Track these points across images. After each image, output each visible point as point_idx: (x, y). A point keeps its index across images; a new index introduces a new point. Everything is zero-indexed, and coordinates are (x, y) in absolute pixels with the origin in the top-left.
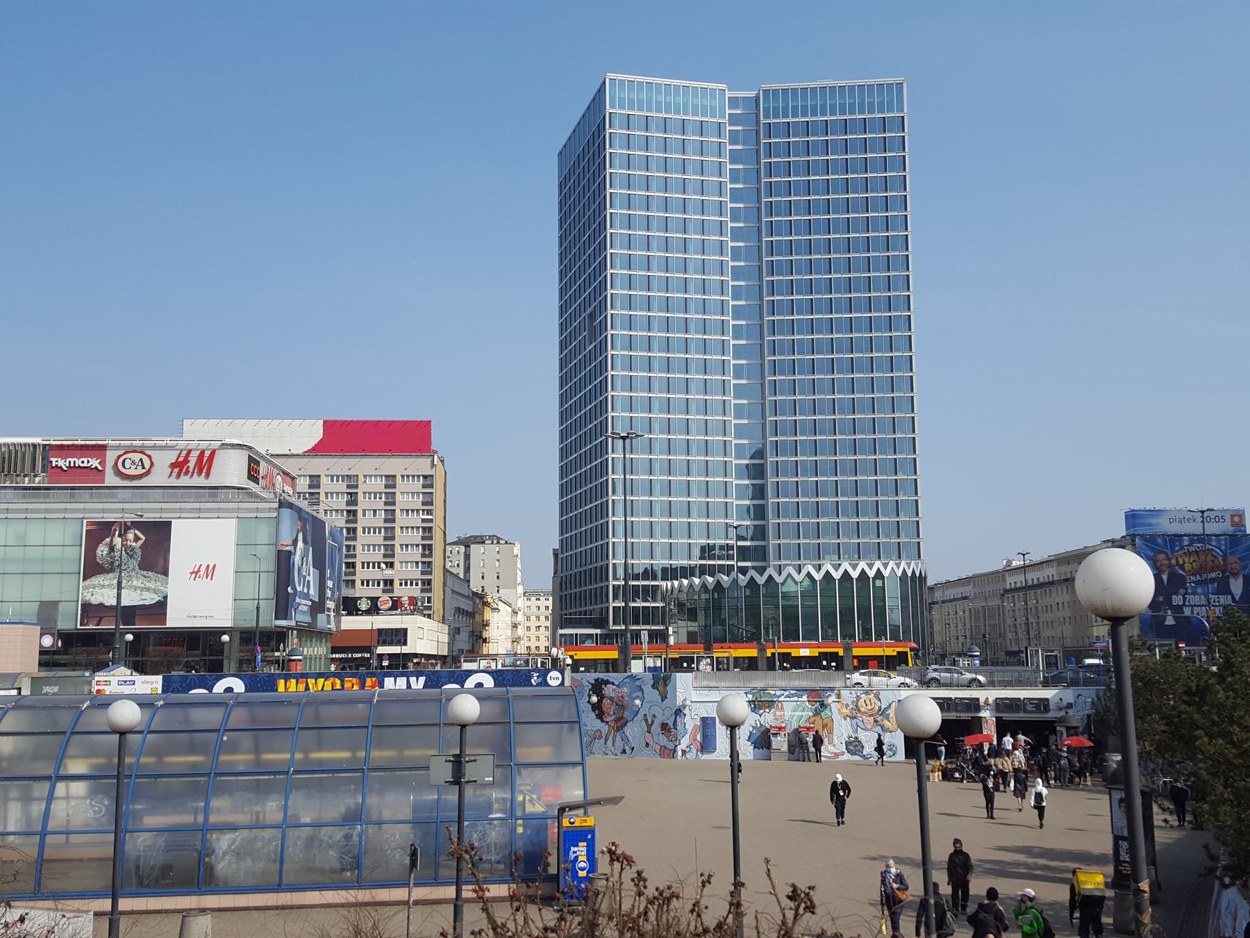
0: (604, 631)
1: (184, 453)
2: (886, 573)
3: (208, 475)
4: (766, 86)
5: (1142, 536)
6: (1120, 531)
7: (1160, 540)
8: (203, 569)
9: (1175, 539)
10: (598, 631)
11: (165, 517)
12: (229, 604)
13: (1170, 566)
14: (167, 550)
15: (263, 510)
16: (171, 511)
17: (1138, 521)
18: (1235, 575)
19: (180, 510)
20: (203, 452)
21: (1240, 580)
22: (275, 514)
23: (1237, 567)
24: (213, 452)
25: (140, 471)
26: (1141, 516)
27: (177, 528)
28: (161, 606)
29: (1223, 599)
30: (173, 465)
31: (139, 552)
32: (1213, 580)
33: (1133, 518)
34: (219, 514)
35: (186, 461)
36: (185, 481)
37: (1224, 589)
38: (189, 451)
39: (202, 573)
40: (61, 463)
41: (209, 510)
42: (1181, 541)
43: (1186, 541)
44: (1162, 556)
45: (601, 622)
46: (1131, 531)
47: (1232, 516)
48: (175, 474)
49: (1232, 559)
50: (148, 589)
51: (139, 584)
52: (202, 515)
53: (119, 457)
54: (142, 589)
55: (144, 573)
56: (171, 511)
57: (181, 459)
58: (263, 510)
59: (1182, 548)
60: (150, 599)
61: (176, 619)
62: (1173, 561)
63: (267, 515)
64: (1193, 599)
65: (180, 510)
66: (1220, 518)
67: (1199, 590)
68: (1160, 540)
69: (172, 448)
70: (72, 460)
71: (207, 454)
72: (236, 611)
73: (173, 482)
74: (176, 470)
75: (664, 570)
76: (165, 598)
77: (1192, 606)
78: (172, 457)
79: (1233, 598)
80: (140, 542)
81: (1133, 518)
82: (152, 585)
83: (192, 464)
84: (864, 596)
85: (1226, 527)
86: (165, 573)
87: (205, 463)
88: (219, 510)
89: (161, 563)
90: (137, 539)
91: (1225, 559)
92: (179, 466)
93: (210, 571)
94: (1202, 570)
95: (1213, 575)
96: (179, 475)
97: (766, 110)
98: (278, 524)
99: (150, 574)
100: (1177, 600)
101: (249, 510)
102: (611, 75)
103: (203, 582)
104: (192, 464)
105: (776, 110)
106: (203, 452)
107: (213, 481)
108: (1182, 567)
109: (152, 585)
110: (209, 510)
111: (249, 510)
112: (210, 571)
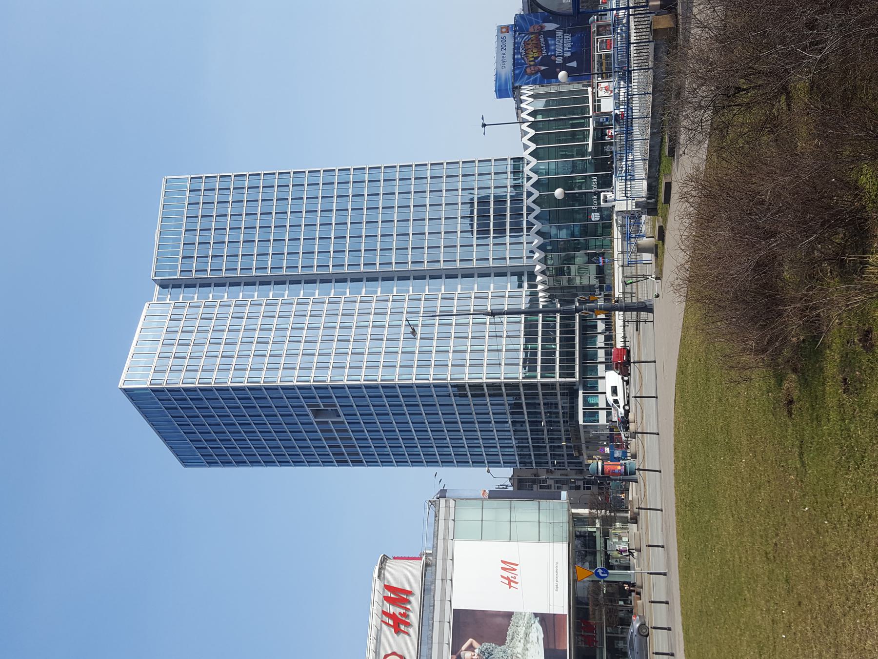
0: (581, 387)
1: (386, 619)
2: (531, 109)
3: (410, 593)
4: (152, 276)
5: (513, 83)
6: (510, 102)
7: (517, 72)
8: (506, 574)
9: (516, 63)
10: (581, 392)
11: (449, 617)
12: (544, 547)
13: (535, 65)
14: (484, 612)
15: (447, 513)
16: (442, 611)
17: (503, 88)
18: (542, 28)
19: (443, 601)
20: (386, 599)
21: (546, 24)
22: (452, 502)
23: (536, 27)
24: (387, 587)
26: (500, 86)
27: (460, 603)
28: (547, 621)
29: (559, 33)
30: (397, 631)
31: (486, 645)
32: (546, 41)
33: (501, 92)
34: (448, 559)
35: (393, 616)
36: (414, 618)
37: (552, 34)
38: (384, 613)
39: (510, 575)
41: (444, 570)
42: (518, 59)
43: (518, 56)
44: (528, 70)
45: (571, 391)
46: (510, 93)
47: (502, 32)
48: (407, 629)
49: (531, 30)
50: (527, 635)
51: (521, 645)
52: (449, 578)
54: (527, 641)
55: (508, 639)
56: (442, 611)
57: (391, 622)
58: (447, 513)
59: (523, 58)
60: (537, 632)
61: (559, 604)
62: (532, 63)
63: (452, 510)
64: (559, 51)
65: (443, 601)
66: (503, 40)
67: (553, 48)
68: (517, 72)
69: (379, 632)
71: (388, 594)
72: (552, 539)
73: (414, 631)
74: (402, 627)
75: (527, 341)
76: (536, 615)
77: (564, 51)
78: (388, 632)
79: (557, 29)
80: (475, 644)
81: (501, 92)
82: (522, 630)
83: (397, 610)
84: (547, 124)
85: (509, 37)
86: (509, 615)
87: (398, 596)
88: (445, 559)
89: (499, 620)
90: (471, 648)
91: (532, 34)
92: (398, 624)
93: (509, 566)
94: (538, 46)
95: (542, 40)
96: (408, 624)
97: (170, 274)
98: (462, 499)
99: (510, 632)
100: (559, 60)
101: (446, 528)
102: (121, 382)
103: (521, 574)
104: (397, 610)
105: (171, 267)
106: (386, 599)
107: (416, 588)
108: (536, 58)
109: (522, 630)
110: (444, 570)
111: (446, 528)
112: (509, 566)
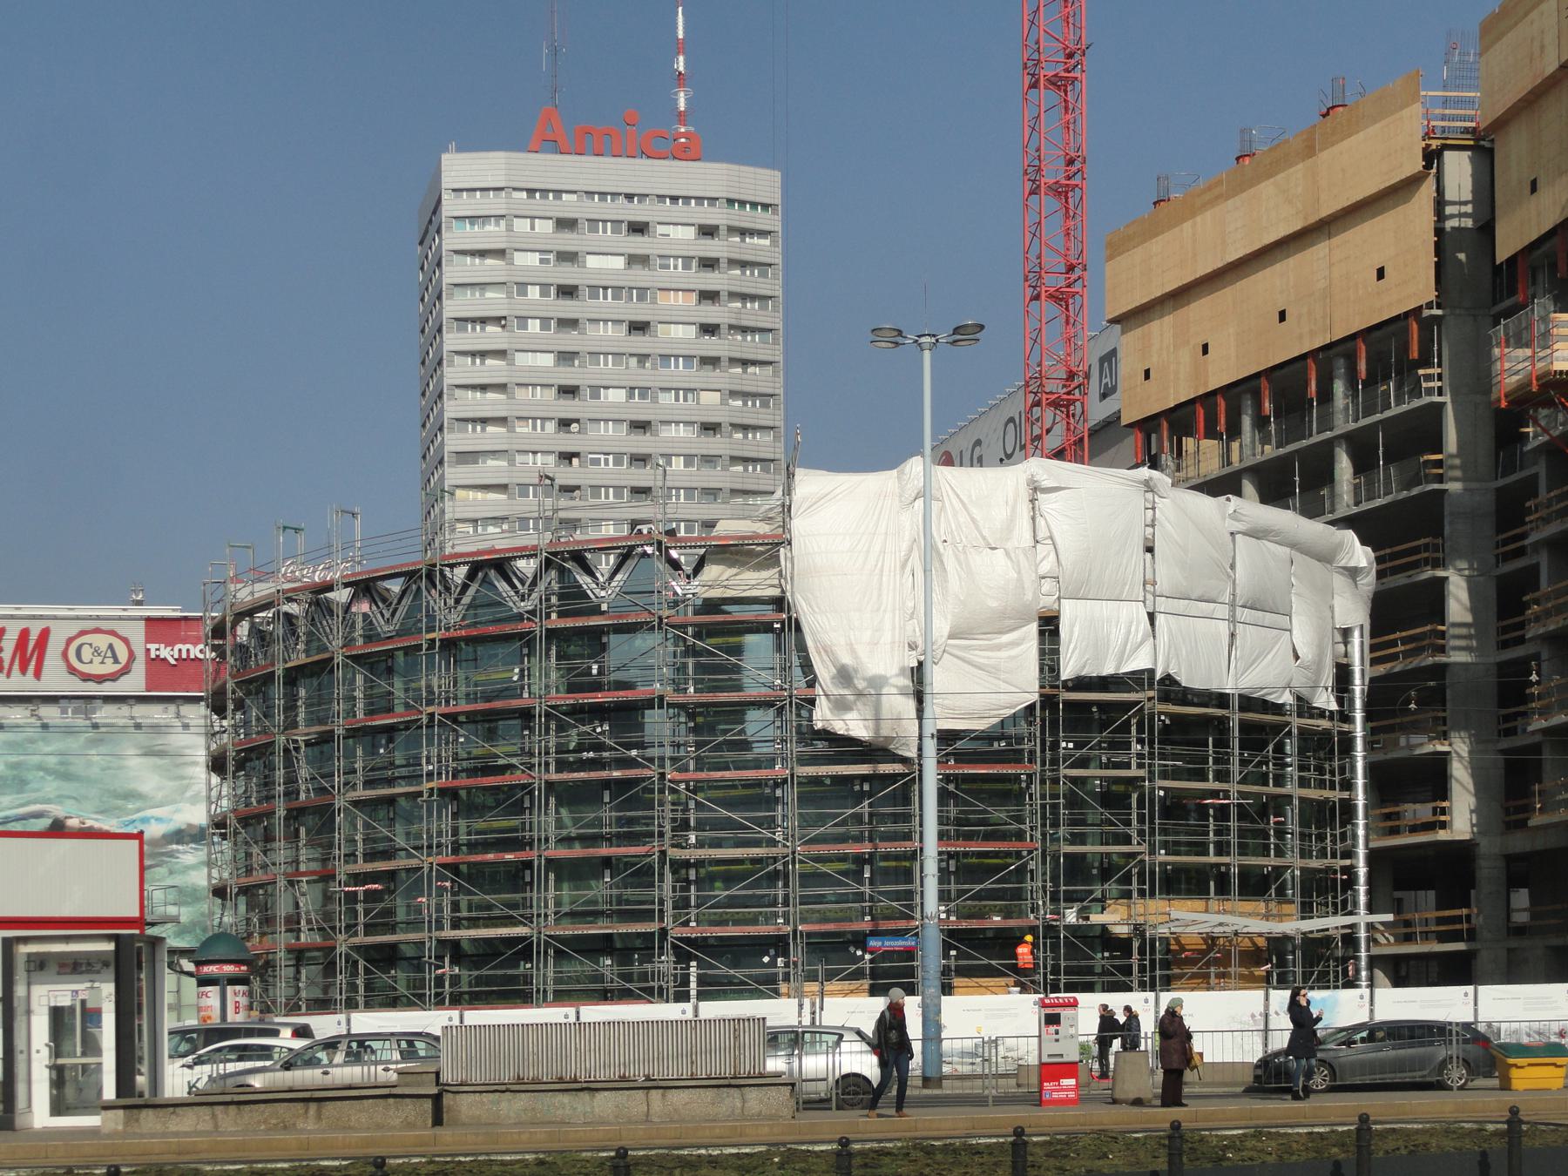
25: (110, 667)
40: (165, 653)
53: (70, 641)
70: (184, 648)
71: (34, 636)
106: (25, 634)
